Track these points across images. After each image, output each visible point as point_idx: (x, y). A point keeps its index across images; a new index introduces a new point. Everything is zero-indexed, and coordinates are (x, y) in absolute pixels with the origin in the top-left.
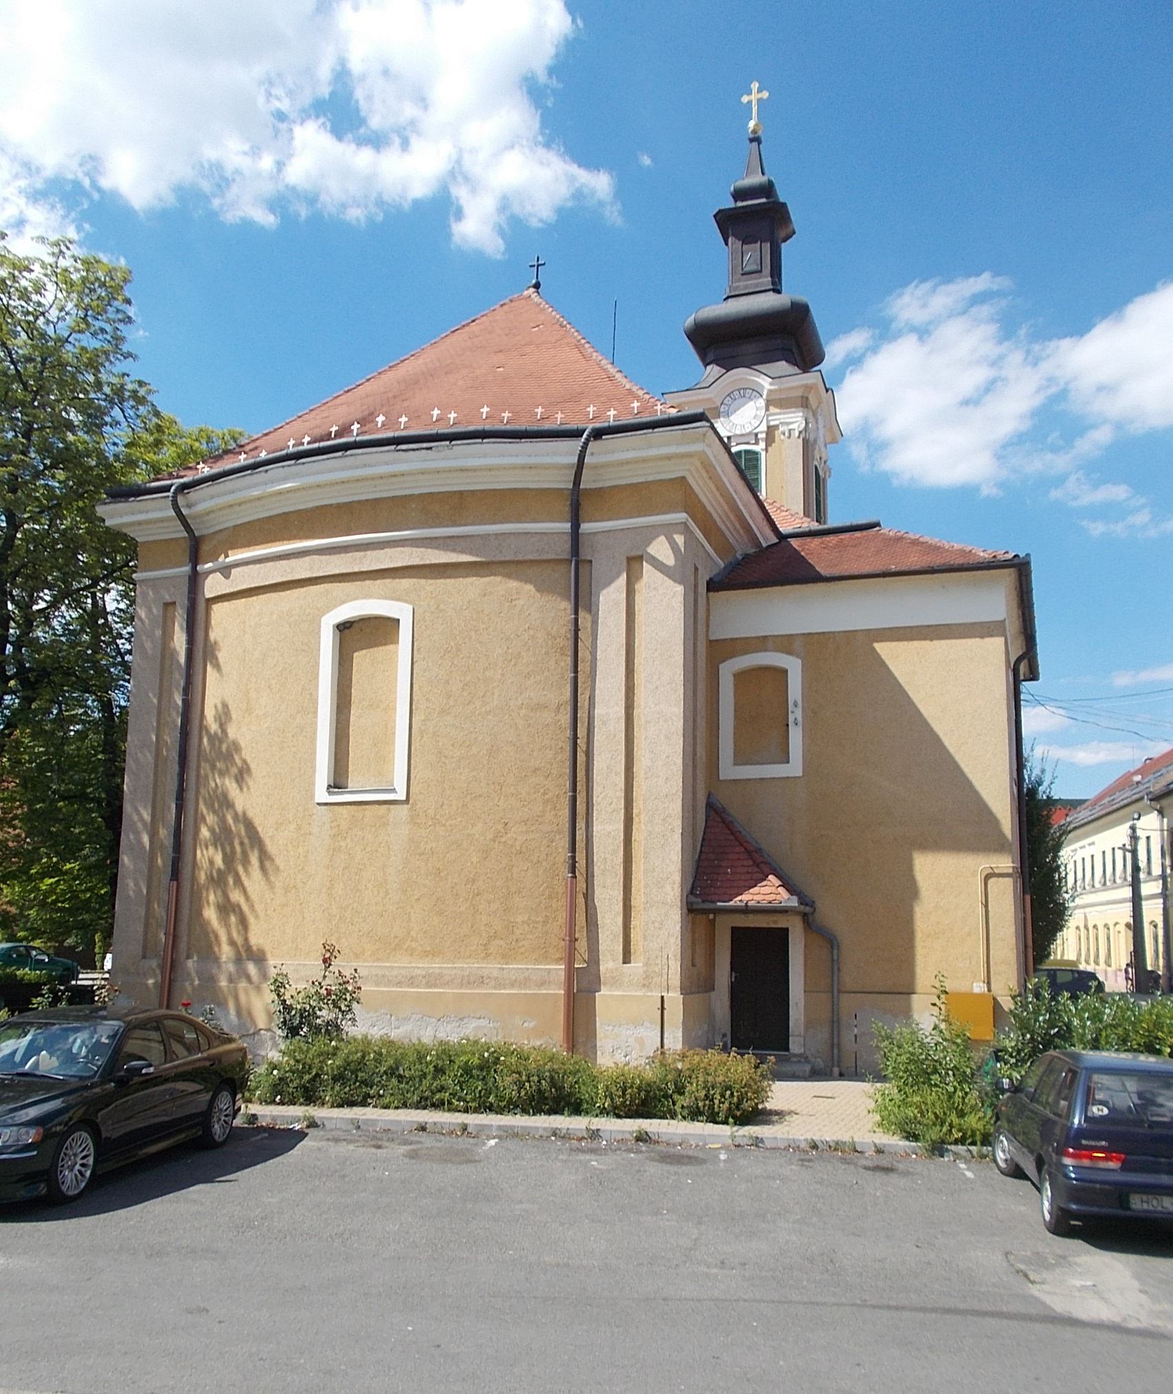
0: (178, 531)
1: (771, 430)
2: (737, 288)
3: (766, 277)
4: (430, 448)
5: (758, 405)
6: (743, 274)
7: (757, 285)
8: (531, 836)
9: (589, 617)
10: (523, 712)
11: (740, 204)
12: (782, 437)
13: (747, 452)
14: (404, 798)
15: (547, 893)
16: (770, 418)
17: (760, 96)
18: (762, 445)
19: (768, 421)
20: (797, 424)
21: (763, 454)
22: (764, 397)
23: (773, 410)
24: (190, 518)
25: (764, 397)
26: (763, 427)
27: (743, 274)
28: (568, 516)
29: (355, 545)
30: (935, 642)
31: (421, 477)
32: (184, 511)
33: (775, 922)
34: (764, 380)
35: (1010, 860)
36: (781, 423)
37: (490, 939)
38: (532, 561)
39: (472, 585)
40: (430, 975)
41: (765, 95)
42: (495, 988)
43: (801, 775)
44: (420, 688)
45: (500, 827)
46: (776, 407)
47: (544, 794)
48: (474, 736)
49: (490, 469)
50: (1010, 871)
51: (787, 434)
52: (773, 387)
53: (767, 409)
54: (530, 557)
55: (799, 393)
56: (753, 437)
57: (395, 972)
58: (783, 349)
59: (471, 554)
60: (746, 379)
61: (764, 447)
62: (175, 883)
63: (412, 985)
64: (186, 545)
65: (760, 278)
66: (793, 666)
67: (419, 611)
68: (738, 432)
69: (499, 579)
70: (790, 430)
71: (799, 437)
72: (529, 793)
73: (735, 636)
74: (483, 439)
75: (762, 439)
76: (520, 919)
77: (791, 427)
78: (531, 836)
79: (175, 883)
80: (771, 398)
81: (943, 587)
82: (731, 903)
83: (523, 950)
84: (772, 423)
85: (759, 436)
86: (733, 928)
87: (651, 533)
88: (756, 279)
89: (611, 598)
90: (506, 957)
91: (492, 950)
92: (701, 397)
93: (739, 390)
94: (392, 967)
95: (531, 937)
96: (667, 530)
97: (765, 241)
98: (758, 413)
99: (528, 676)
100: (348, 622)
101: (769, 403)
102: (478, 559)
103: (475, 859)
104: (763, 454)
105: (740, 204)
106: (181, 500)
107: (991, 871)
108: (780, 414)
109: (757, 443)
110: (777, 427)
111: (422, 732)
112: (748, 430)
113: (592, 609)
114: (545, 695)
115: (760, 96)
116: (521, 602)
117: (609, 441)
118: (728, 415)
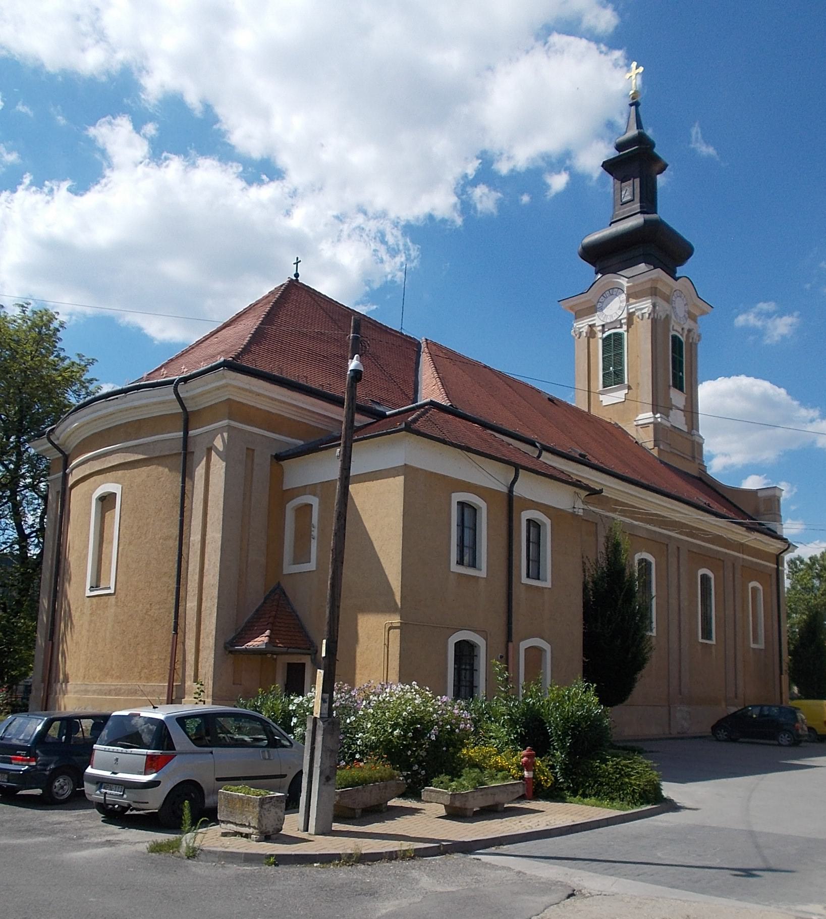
0: (56, 455)
1: (630, 316)
2: (617, 216)
3: (637, 203)
4: (117, 398)
5: (621, 299)
6: (622, 205)
7: (630, 211)
8: (161, 611)
9: (191, 483)
10: (161, 541)
11: (621, 153)
12: (638, 320)
13: (615, 334)
14: (113, 592)
15: (166, 643)
16: (629, 307)
17: (638, 71)
18: (625, 327)
19: (628, 309)
20: (647, 309)
21: (626, 334)
22: (625, 292)
23: (632, 301)
24: (60, 445)
25: (625, 292)
26: (625, 315)
27: (622, 205)
28: (182, 429)
29: (102, 454)
30: (374, 482)
31: (120, 414)
32: (56, 443)
33: (300, 660)
34: (623, 280)
35: (399, 618)
36: (636, 310)
37: (142, 668)
38: (168, 455)
39: (144, 471)
40: (116, 689)
41: (641, 69)
42: (141, 696)
43: (315, 569)
44: (123, 531)
45: (148, 606)
46: (633, 298)
47: (168, 587)
48: (141, 556)
49: (147, 406)
50: (399, 625)
51: (640, 317)
52: (629, 284)
53: (628, 300)
54: (167, 453)
55: (649, 285)
56: (619, 322)
57: (105, 687)
58: (643, 254)
59: (143, 454)
60: (611, 281)
61: (626, 329)
62: (51, 642)
63: (109, 695)
64: (62, 462)
65: (634, 205)
66: (314, 501)
67: (124, 488)
68: (608, 321)
69: (154, 467)
70: (643, 314)
71: (649, 318)
72: (161, 587)
73: (294, 487)
74: (138, 390)
75: (624, 323)
76: (155, 657)
77: (643, 311)
78: (161, 611)
79: (51, 642)
80: (630, 292)
81: (378, 447)
82: (243, 647)
83: (155, 675)
84: (631, 311)
85: (622, 321)
86: (289, 664)
87: (213, 434)
88: (631, 206)
89: (200, 471)
90: (148, 679)
91: (142, 675)
92: (578, 301)
93: (609, 290)
94: (103, 685)
95: (158, 667)
96: (220, 430)
97: (637, 178)
98: (621, 305)
99: (163, 521)
100: (103, 496)
101: (629, 296)
102: (141, 457)
103: (138, 625)
104: (626, 334)
105: (621, 153)
106: (52, 438)
107: (390, 625)
108: (636, 303)
109: (621, 327)
110: (633, 313)
111: (122, 555)
112: (614, 319)
113: (192, 478)
114: (171, 531)
115: (638, 71)
116: (163, 479)
117: (192, 383)
118: (602, 310)
